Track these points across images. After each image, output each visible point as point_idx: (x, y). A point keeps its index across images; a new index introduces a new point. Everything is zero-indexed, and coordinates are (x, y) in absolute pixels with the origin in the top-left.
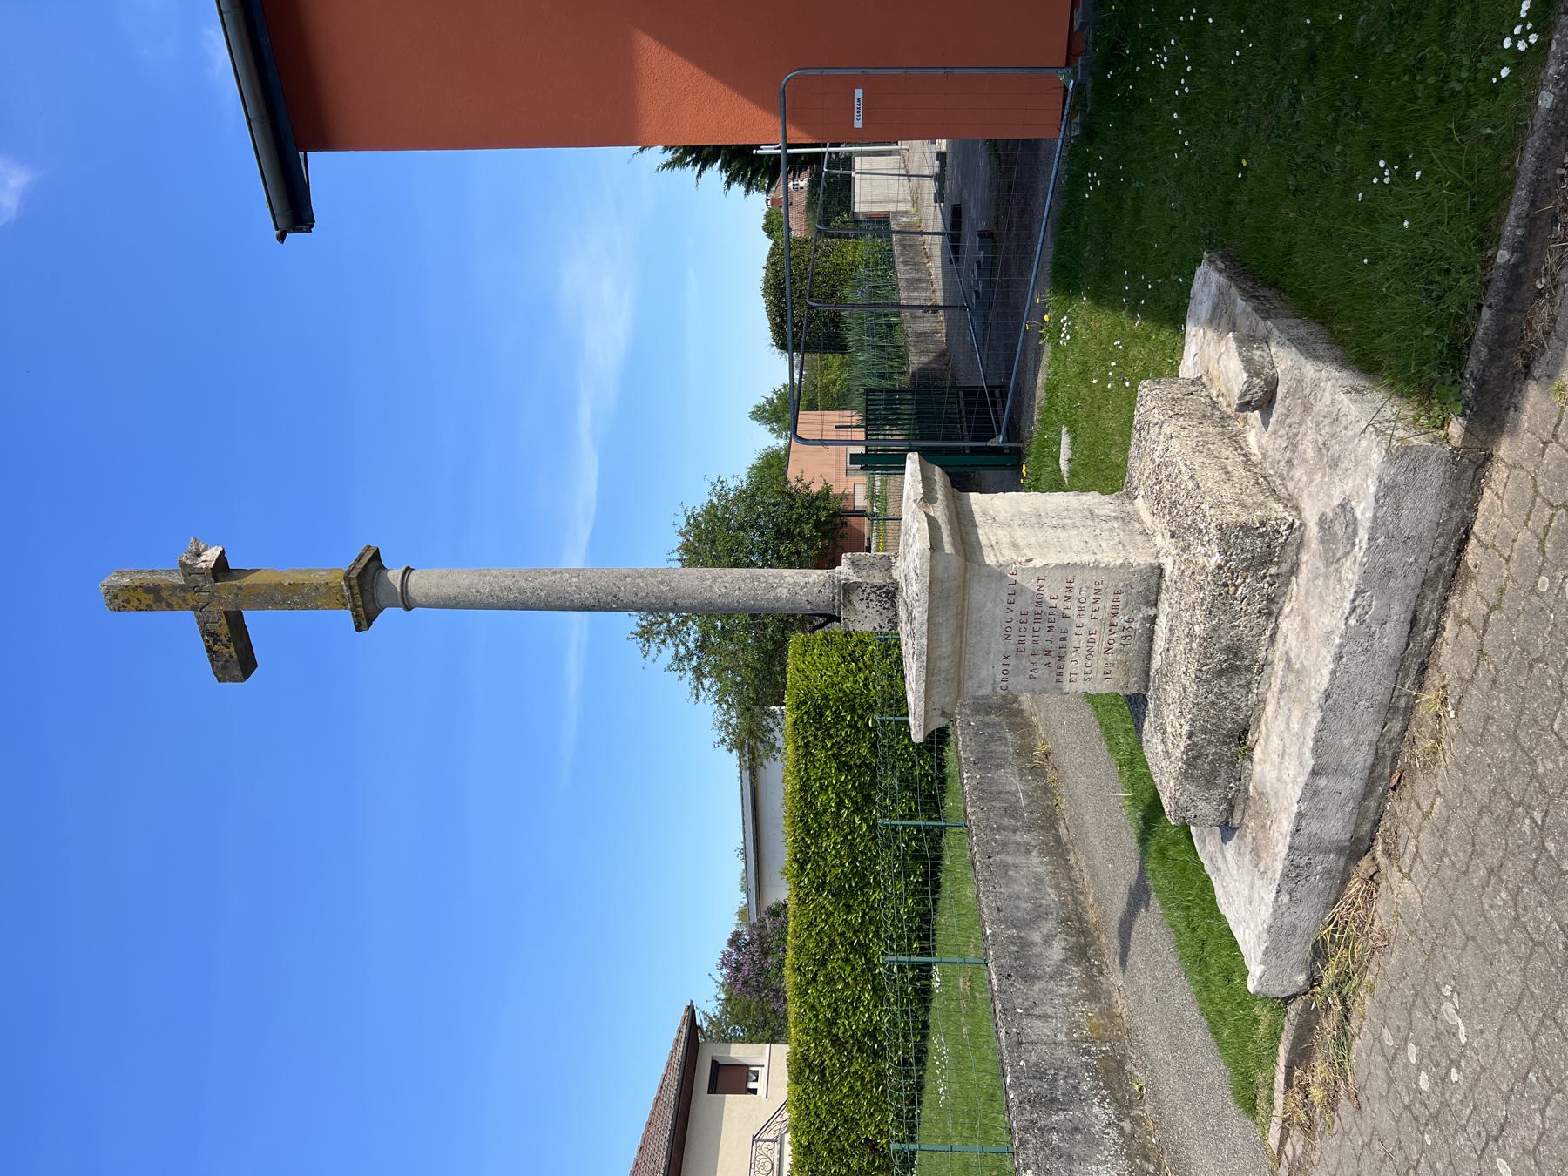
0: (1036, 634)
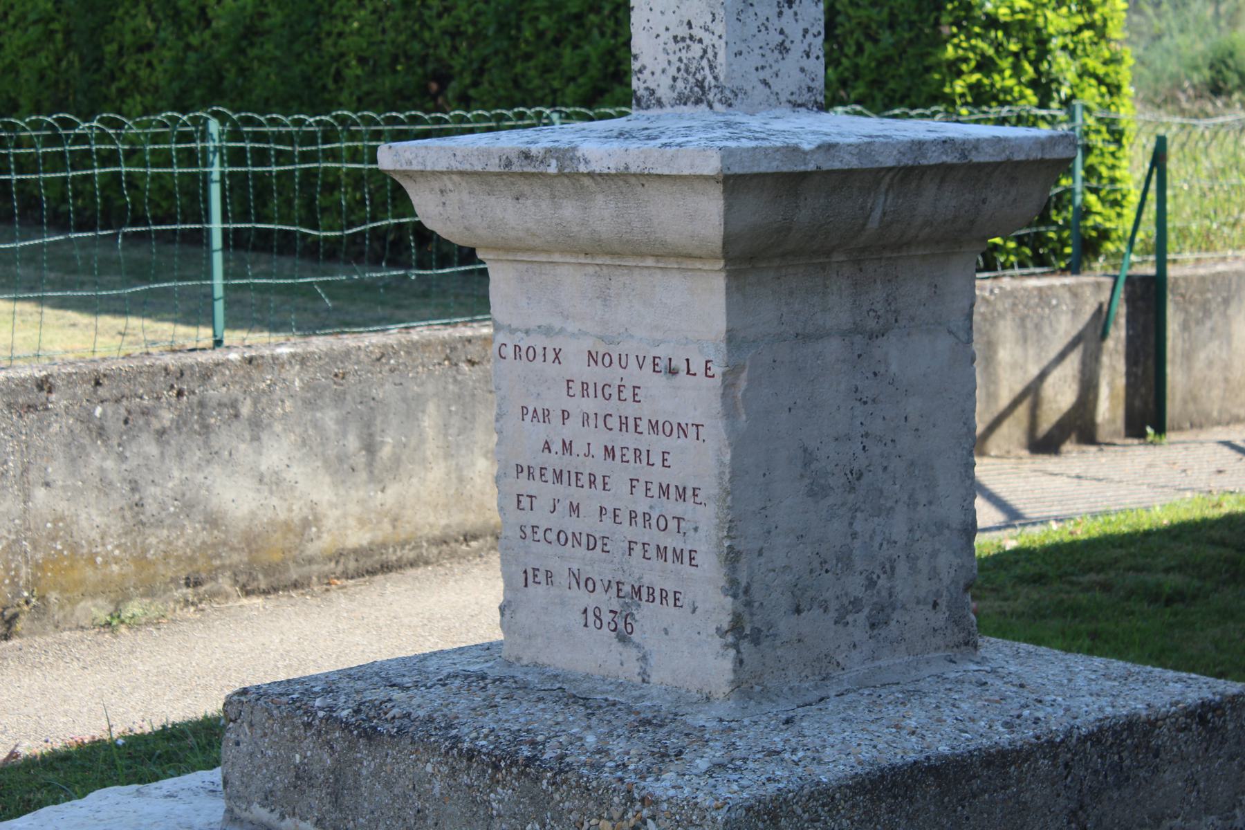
0: (600, 422)
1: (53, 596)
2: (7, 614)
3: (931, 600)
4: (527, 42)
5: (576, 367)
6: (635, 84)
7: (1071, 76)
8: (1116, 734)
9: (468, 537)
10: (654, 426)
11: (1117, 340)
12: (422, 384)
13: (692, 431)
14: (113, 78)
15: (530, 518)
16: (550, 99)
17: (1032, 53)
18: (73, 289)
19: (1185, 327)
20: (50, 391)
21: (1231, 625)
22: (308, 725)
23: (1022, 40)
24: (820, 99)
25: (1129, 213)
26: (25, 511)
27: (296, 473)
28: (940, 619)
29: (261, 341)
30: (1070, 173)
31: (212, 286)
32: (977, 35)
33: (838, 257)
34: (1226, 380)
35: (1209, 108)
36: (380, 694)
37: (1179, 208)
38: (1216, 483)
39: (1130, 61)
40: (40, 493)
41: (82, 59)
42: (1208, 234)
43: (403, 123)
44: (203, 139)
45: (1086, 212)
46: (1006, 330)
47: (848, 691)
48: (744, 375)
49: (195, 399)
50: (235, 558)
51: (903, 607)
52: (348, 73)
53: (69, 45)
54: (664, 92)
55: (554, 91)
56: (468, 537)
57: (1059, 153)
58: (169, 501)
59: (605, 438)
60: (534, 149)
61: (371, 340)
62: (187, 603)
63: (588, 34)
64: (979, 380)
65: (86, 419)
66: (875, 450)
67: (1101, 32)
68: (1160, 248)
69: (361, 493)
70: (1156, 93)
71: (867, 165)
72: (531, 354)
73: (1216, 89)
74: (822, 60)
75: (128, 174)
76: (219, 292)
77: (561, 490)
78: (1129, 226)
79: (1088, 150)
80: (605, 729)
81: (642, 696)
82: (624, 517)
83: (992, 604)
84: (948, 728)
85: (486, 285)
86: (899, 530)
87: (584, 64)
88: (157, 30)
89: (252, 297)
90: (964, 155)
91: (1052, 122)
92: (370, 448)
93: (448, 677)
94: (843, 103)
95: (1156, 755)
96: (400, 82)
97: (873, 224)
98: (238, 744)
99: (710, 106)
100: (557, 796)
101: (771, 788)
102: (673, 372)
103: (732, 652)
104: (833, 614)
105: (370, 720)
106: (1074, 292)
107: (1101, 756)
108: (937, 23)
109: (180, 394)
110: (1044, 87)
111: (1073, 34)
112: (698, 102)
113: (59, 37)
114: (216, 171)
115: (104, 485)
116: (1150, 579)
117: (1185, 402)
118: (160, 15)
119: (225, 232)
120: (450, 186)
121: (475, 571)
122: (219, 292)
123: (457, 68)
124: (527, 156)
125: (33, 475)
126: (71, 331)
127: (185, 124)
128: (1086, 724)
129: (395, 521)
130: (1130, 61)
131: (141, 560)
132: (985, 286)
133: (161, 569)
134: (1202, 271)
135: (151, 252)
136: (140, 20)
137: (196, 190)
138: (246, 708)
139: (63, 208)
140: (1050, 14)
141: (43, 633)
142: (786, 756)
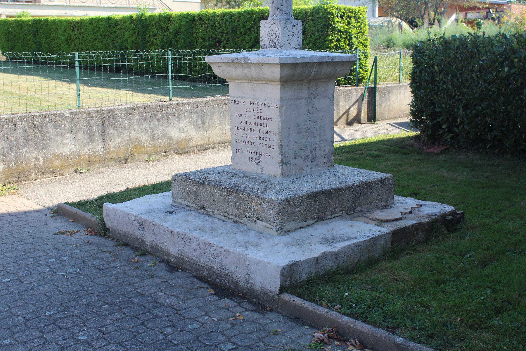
1: (136, 154)
3: (324, 156)
4: (238, 34)
6: (261, 43)
7: (356, 43)
10: (264, 118)
11: (366, 101)
13: (273, 119)
14: (148, 42)
15: (238, 138)
16: (243, 47)
17: (348, 38)
18: (139, 88)
19: (380, 98)
21: (388, 162)
22: (190, 182)
24: (301, 47)
25: (369, 73)
27: (187, 128)
29: (180, 100)
30: (356, 64)
32: (336, 34)
33: (305, 81)
34: (389, 110)
35: (386, 51)
36: (205, 176)
37: (380, 72)
38: (386, 132)
39: (369, 40)
40: (133, 132)
41: (141, 38)
45: (360, 73)
46: (342, 98)
48: (284, 107)
50: (174, 146)
51: (318, 158)
52: (199, 41)
53: (139, 35)
54: (267, 45)
55: (244, 45)
57: (353, 59)
58: (160, 134)
60: (239, 57)
61: (204, 99)
63: (252, 33)
64: (335, 109)
65: (142, 116)
66: (312, 124)
70: (375, 47)
72: (238, 102)
74: (302, 38)
75: (151, 63)
76: (171, 89)
77: (244, 132)
78: (369, 76)
79: (360, 59)
82: (258, 138)
83: (337, 158)
84: (327, 183)
85: (228, 88)
86: (317, 141)
87: (250, 39)
89: (178, 90)
91: (352, 53)
92: (203, 123)
94: (307, 48)
95: (371, 189)
96: (210, 43)
97: (313, 74)
99: (277, 48)
100: (243, 198)
101: (289, 196)
102: (269, 106)
103: (281, 167)
104: (303, 159)
105: (203, 181)
106: (357, 91)
108: (328, 31)
109: (162, 111)
110: (351, 45)
111: (357, 34)
112: (275, 47)
113: (136, 33)
114: (170, 62)
115: (146, 130)
116: (371, 152)
117: (380, 115)
118: (158, 28)
119: (172, 76)
120: (221, 65)
121: (226, 150)
122: (171, 89)
123: (223, 40)
124: (237, 59)
125: (131, 128)
127: (163, 52)
128: (356, 183)
130: (369, 40)
131: (154, 147)
132: (337, 89)
133: (159, 149)
134: (384, 86)
135: (156, 80)
136: (154, 29)
137: (166, 67)
138: (177, 178)
139: (137, 71)
140: (352, 29)
141: (134, 162)
142: (292, 189)
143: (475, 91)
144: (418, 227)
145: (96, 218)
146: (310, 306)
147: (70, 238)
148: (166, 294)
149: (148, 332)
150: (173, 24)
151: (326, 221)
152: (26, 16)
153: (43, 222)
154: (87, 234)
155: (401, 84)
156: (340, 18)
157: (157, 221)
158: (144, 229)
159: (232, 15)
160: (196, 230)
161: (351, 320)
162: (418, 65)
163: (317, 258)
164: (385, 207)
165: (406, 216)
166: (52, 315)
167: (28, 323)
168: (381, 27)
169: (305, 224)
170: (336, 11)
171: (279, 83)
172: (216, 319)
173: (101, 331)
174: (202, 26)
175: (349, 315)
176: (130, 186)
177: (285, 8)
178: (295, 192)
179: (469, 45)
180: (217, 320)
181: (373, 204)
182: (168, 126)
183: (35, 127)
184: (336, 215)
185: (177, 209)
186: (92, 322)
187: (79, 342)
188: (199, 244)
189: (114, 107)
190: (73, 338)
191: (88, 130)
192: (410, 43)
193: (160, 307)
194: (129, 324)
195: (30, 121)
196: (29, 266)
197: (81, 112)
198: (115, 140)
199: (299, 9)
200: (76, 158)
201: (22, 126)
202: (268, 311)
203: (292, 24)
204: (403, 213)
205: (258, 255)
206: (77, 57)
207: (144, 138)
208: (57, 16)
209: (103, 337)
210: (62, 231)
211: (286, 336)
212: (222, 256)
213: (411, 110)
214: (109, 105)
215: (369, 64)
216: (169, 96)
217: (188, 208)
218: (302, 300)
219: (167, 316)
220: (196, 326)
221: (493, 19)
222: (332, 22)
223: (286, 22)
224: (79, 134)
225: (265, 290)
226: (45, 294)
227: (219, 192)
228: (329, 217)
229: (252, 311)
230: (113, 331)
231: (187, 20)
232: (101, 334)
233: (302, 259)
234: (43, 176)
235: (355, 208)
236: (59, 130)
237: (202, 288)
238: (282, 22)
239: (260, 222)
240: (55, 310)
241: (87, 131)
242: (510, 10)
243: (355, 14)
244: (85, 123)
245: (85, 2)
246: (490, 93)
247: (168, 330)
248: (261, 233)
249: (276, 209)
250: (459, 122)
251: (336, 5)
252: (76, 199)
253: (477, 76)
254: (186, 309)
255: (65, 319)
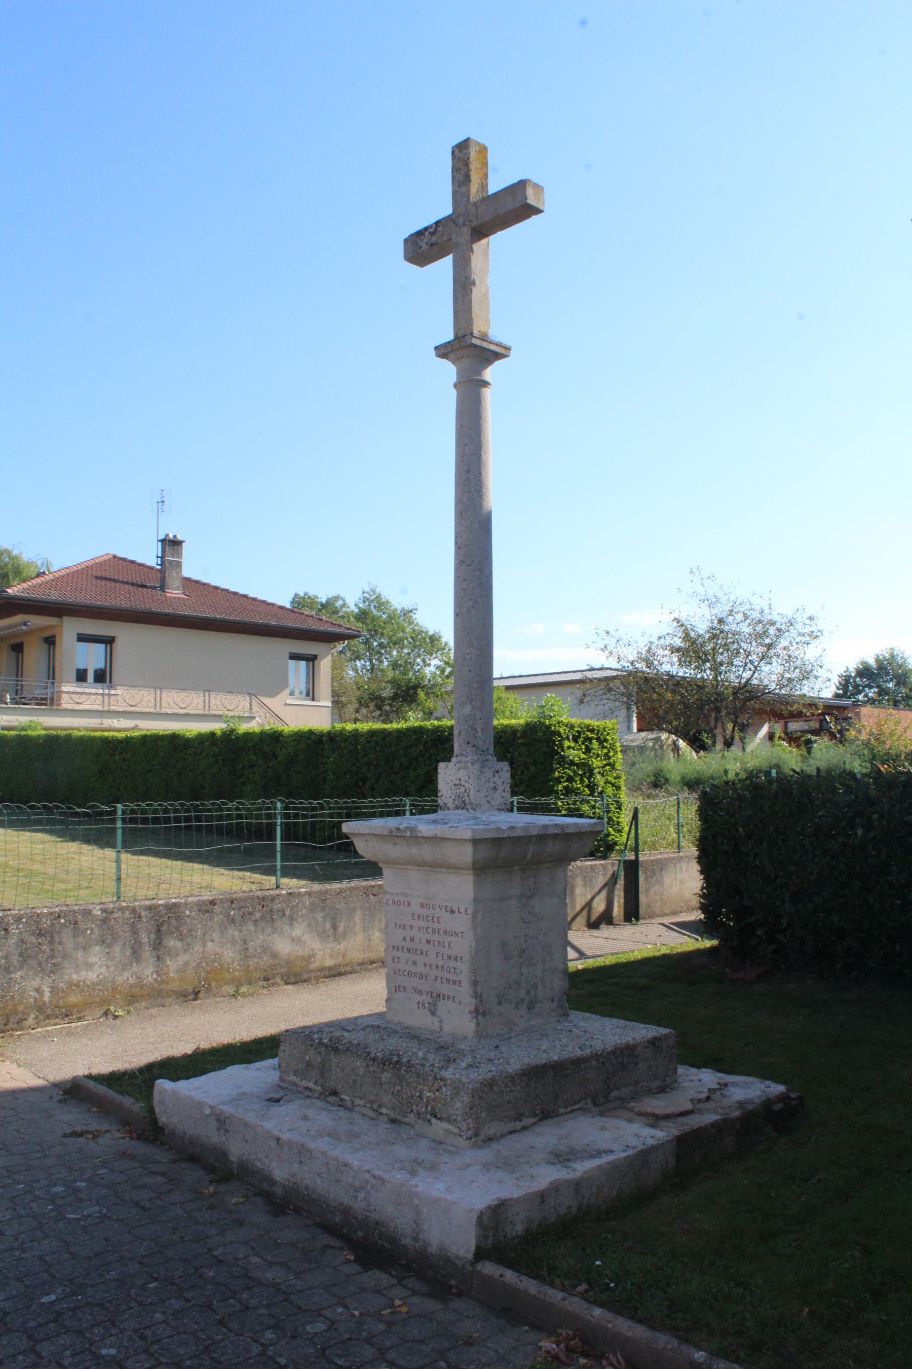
0: (425, 931)
1: (213, 984)
2: (196, 990)
5: (416, 908)
7: (602, 783)
8: (622, 1051)
9: (372, 962)
10: (445, 932)
11: (621, 885)
12: (355, 903)
13: (460, 935)
19: (646, 879)
20: (214, 905)
23: (583, 770)
25: (625, 835)
26: (204, 951)
27: (306, 937)
28: (554, 1005)
31: (276, 865)
32: (567, 768)
33: (516, 868)
34: (662, 899)
35: (653, 793)
40: (210, 944)
42: (654, 843)
43: (349, 803)
44: (275, 809)
45: (609, 835)
46: (579, 881)
47: (519, 1034)
48: (480, 914)
49: (269, 909)
50: (282, 970)
51: (540, 1001)
54: (450, 805)
56: (372, 962)
59: (427, 936)
60: (401, 827)
61: (336, 886)
62: (264, 987)
67: (613, 766)
68: (636, 850)
69: (331, 945)
71: (527, 834)
72: (398, 903)
73: (656, 785)
80: (426, 1050)
81: (440, 1037)
82: (434, 967)
88: (257, 760)
90: (563, 830)
92: (335, 927)
93: (365, 1027)
97: (529, 856)
98: (284, 1051)
99: (468, 810)
100: (407, 1077)
101: (490, 1074)
102: (453, 912)
103: (475, 1020)
107: (616, 1059)
108: (552, 764)
109: (263, 906)
110: (592, 787)
112: (463, 809)
113: (221, 762)
114: (279, 821)
115: (234, 941)
121: (374, 976)
124: (398, 829)
125: (207, 937)
126: (221, 877)
127: (268, 804)
129: (344, 956)
131: (247, 971)
137: (271, 828)
142: (496, 1061)
143: (809, 870)
144: (721, 1127)
145: (141, 1106)
146: (530, 1286)
147: (92, 1144)
148: (266, 1260)
149: (231, 1339)
150: (284, 747)
151: (556, 1119)
152: (35, 729)
153: (45, 1111)
154: (123, 1138)
155: (681, 854)
156: (572, 742)
157: (251, 1117)
158: (227, 1131)
159: (384, 733)
160: (321, 1136)
161: (608, 1315)
162: (709, 824)
163: (543, 1191)
164: (663, 1089)
165: (701, 1105)
166: (53, 1302)
167: (8, 1319)
168: (642, 749)
169: (518, 1125)
170: (565, 730)
171: (472, 871)
172: (357, 1313)
173: (143, 1337)
174: (334, 752)
175: (601, 1305)
176: (203, 1043)
177: (480, 743)
178: (501, 1067)
179: (795, 792)
180: (360, 1314)
181: (641, 1084)
182: (273, 933)
183: (40, 935)
184: (574, 1107)
185: (288, 1093)
186: (128, 1318)
187: (101, 1361)
188: (327, 1164)
189: (179, 900)
190: (90, 1351)
191: (130, 941)
192: (694, 778)
193: (254, 1287)
194: (197, 1323)
195: (32, 923)
196: (17, 1201)
197: (121, 909)
198: (178, 959)
199: (502, 725)
200: (107, 990)
201: (17, 931)
202: (453, 1295)
203: (493, 770)
204: (695, 1102)
205: (436, 1186)
206: (119, 812)
207: (229, 954)
208: (86, 729)
209: (146, 1351)
210: (79, 1129)
211: (488, 1348)
212: (369, 1187)
213: (701, 903)
214: (170, 896)
215: (625, 819)
216: (276, 876)
217: (308, 1093)
218: (517, 1274)
219: (267, 1307)
220: (320, 1326)
221: (832, 736)
222: (558, 747)
223: (483, 766)
224: (115, 947)
225: (448, 1254)
226: (41, 1258)
227: (364, 1064)
228: (562, 1111)
229: (423, 1295)
230: (166, 1338)
231: (309, 742)
232: (141, 1343)
233: (516, 1194)
234: (47, 1021)
235: (609, 1093)
236: (80, 939)
237: (333, 1247)
238: (476, 766)
239: (439, 1122)
240: (59, 1291)
241: (130, 941)
242: (860, 720)
243: (598, 734)
244: (127, 928)
245: (134, 706)
246: (836, 872)
247: (269, 1335)
248: (440, 1143)
249: (466, 1099)
250: (785, 924)
251: (565, 719)
252: (104, 1067)
253: (812, 843)
254: (300, 1291)
255: (78, 1311)
